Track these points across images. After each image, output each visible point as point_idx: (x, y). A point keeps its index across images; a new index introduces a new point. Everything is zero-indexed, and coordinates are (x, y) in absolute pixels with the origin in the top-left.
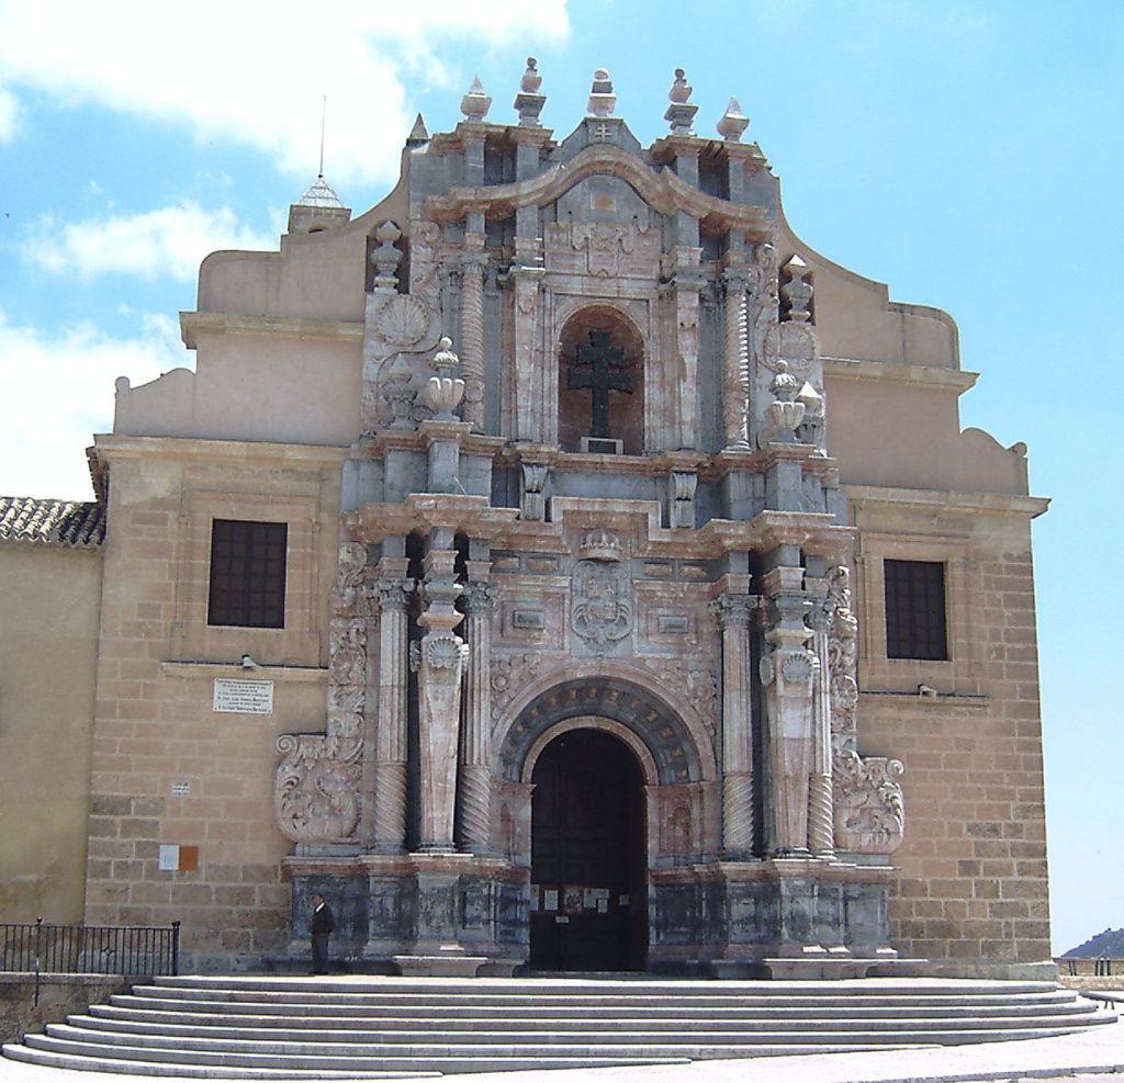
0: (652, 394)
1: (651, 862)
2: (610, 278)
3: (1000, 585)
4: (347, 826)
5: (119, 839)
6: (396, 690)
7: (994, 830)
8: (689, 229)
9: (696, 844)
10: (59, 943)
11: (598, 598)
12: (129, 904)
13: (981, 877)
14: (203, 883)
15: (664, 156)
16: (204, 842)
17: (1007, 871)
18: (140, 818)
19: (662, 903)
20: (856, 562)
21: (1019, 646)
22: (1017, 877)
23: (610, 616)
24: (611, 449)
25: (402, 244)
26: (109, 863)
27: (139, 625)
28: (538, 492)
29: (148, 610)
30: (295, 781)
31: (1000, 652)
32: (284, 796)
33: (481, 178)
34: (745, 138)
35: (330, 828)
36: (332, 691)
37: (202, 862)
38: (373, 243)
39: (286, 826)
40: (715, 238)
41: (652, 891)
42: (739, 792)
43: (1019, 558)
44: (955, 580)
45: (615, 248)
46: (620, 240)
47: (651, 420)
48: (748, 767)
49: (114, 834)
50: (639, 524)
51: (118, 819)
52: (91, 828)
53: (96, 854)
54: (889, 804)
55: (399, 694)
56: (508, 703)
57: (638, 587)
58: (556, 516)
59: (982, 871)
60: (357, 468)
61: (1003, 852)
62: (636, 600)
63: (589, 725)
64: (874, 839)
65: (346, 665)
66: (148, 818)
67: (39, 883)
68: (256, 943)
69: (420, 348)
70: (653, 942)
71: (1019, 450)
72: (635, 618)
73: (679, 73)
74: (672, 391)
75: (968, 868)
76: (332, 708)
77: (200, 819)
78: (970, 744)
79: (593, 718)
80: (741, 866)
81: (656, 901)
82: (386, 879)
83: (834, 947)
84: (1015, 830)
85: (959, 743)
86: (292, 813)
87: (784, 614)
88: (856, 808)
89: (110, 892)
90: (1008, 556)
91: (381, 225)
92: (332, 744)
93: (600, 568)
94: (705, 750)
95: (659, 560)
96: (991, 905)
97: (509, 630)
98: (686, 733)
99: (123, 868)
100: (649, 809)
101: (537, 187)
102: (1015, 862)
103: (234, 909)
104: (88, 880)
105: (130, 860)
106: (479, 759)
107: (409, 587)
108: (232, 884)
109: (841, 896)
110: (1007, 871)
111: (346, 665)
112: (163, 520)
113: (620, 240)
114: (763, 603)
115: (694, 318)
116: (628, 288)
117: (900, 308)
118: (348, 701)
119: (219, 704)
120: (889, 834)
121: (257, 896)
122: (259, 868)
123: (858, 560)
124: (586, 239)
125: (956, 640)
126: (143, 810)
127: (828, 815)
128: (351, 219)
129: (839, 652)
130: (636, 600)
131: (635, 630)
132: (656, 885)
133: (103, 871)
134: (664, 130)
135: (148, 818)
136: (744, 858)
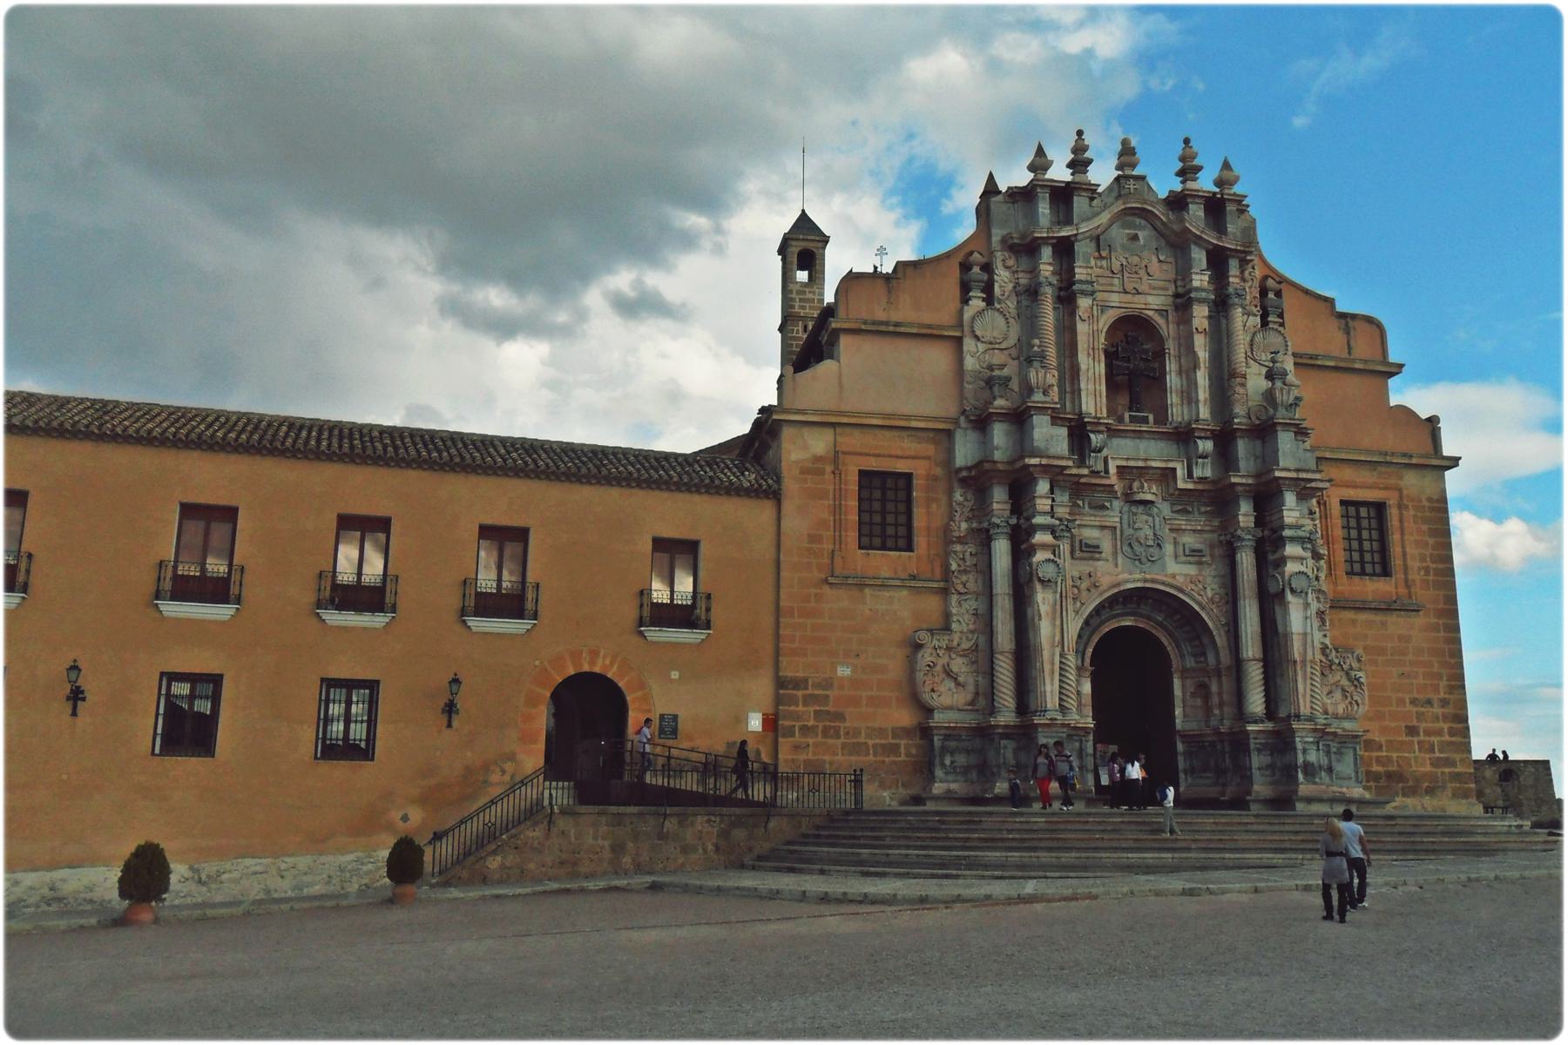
4: (970, 697)
7: (1429, 702)
8: (1199, 257)
12: (810, 756)
13: (1422, 737)
15: (1177, 202)
17: (1439, 733)
19: (1188, 754)
22: (1447, 738)
24: (1145, 420)
25: (988, 268)
29: (814, 538)
33: (1032, 229)
34: (1238, 189)
38: (965, 267)
40: (1218, 261)
41: (1180, 747)
43: (1438, 501)
48: (1259, 655)
51: (800, 693)
58: (1112, 470)
61: (1437, 719)
73: (1187, 141)
74: (1188, 378)
75: (1412, 731)
76: (954, 611)
78: (1407, 639)
84: (1444, 703)
85: (1401, 638)
89: (796, 748)
90: (1430, 500)
91: (971, 253)
93: (1141, 509)
94: (1221, 640)
97: (1078, 554)
99: (806, 730)
102: (1446, 726)
105: (810, 723)
107: (1014, 521)
110: (1439, 733)
112: (820, 472)
115: (1205, 324)
116: (1153, 302)
117: (1343, 316)
118: (966, 605)
121: (902, 750)
122: (904, 729)
126: (818, 685)
133: (790, 732)
134: (1176, 185)
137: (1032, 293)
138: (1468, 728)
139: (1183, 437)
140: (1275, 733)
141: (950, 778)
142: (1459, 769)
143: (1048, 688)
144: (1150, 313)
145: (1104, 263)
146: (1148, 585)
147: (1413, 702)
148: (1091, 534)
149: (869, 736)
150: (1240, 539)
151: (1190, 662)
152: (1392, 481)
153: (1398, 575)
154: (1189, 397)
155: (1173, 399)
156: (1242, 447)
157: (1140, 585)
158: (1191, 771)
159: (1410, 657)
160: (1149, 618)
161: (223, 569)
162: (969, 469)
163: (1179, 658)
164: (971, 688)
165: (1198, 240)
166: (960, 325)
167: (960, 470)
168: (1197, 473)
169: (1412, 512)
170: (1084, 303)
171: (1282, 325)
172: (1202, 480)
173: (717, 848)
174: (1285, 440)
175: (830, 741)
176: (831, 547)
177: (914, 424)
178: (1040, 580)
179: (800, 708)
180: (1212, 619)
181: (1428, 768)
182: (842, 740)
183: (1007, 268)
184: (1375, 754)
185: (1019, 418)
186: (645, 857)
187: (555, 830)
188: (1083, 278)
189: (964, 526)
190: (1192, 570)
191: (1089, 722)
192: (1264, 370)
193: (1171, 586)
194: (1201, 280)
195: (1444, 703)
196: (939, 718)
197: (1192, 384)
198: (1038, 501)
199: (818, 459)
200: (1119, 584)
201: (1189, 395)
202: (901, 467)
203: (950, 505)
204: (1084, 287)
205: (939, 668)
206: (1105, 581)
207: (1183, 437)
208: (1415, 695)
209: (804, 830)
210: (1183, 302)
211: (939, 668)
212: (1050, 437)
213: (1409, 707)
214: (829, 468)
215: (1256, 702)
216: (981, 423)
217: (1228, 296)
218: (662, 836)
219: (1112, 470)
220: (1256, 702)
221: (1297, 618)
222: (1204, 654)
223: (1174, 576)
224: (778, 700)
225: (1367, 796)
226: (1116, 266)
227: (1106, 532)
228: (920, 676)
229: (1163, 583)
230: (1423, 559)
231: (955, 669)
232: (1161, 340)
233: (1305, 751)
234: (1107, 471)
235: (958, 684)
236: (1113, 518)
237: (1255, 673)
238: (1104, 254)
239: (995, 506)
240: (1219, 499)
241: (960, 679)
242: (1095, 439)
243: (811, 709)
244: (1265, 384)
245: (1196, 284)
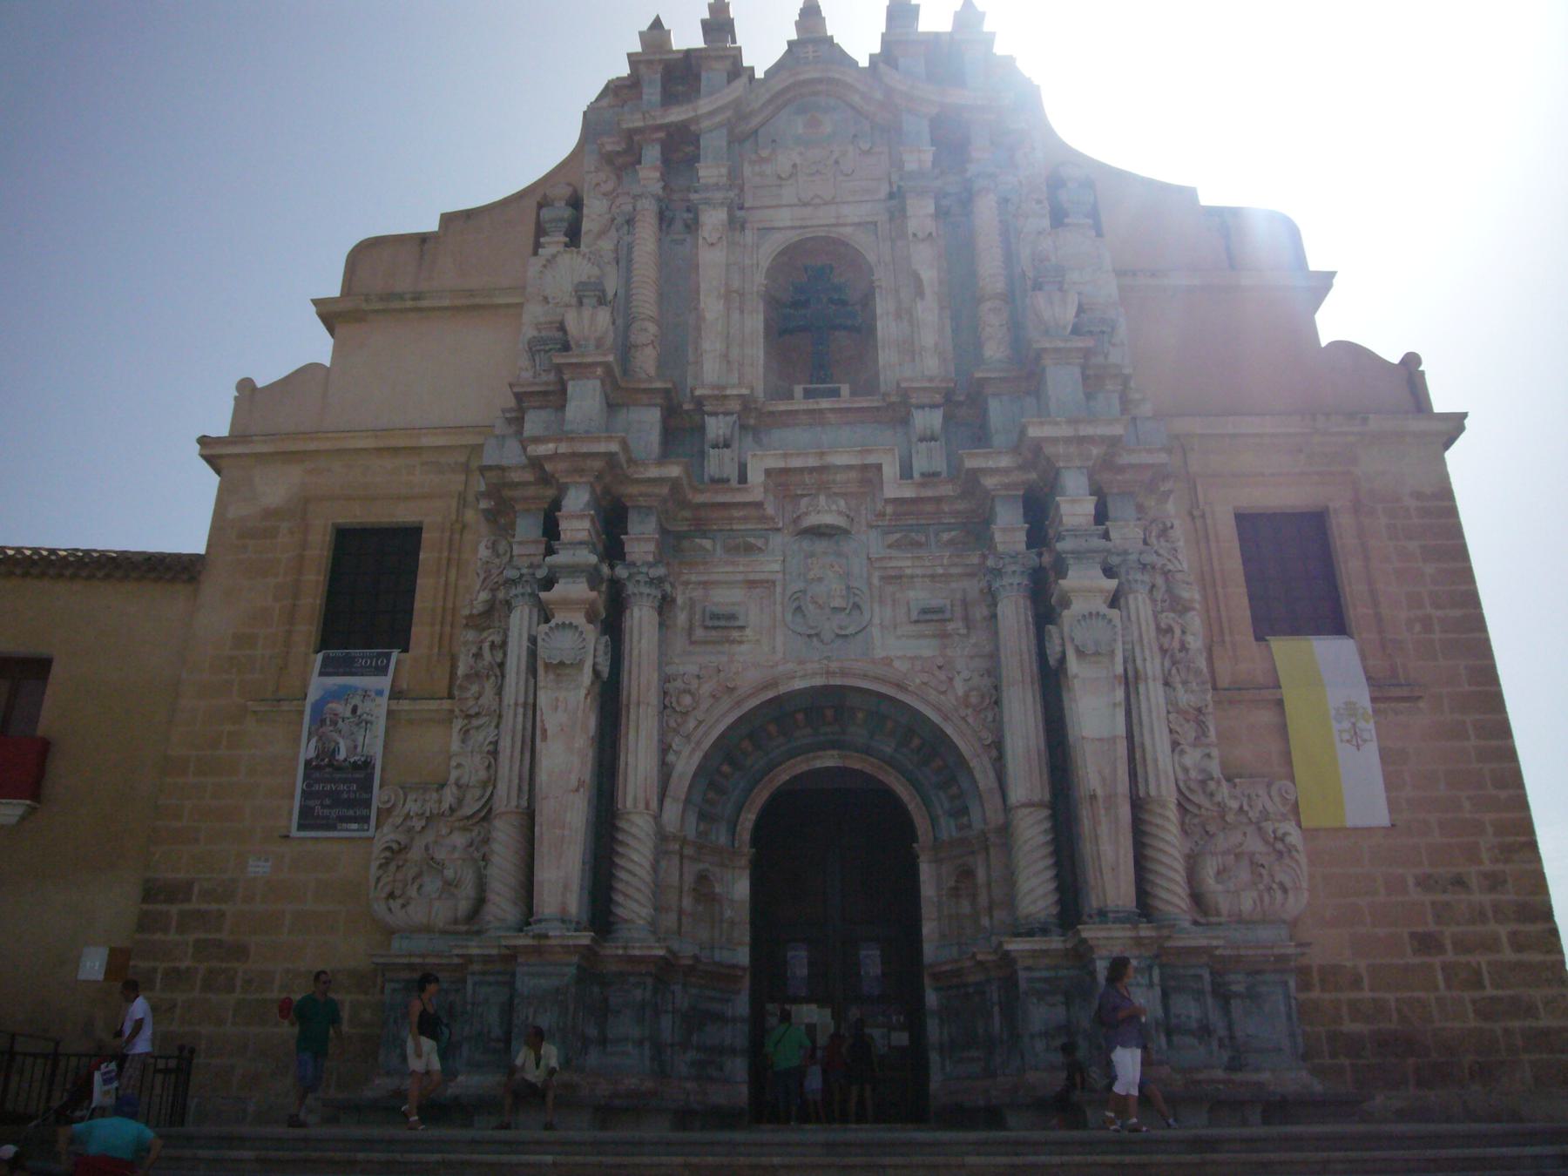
0: (887, 328)
2: (826, 203)
4: (464, 906)
5: (173, 936)
6: (521, 710)
9: (985, 921)
11: (820, 580)
13: (1450, 956)
17: (1491, 945)
18: (204, 906)
20: (1193, 518)
22: (1509, 955)
23: (838, 603)
25: (576, 203)
26: (155, 970)
28: (727, 445)
30: (395, 846)
32: (381, 866)
35: (442, 913)
36: (458, 724)
39: (380, 908)
41: (932, 998)
42: (1032, 832)
46: (837, 162)
47: (886, 357)
48: (1042, 793)
50: (870, 475)
51: (174, 909)
54: (1279, 846)
55: (525, 715)
56: (696, 728)
57: (877, 565)
58: (756, 476)
59: (1449, 947)
62: (876, 581)
63: (830, 763)
64: (1262, 900)
65: (475, 688)
66: (214, 906)
71: (1411, 361)
72: (876, 608)
79: (835, 752)
80: (1036, 943)
82: (491, 979)
84: (1494, 882)
86: (387, 889)
87: (1071, 561)
88: (1227, 852)
90: (1418, 495)
92: (449, 796)
93: (821, 545)
96: (1474, 1002)
97: (699, 633)
98: (962, 762)
100: (922, 878)
101: (720, 103)
102: (1503, 931)
105: (183, 965)
106: (635, 799)
109: (1208, 988)
111: (475, 688)
113: (837, 162)
114: (1047, 559)
120: (1285, 890)
123: (1196, 513)
124: (794, 166)
127: (1176, 870)
129: (1178, 632)
130: (876, 581)
131: (876, 621)
132: (936, 989)
135: (214, 906)
136: (1044, 931)
138: (1554, 932)
142: (1545, 1022)
146: (837, 681)
147: (1425, 883)
160: (868, 751)
161: (901, 1038)
172: (930, 477)
181: (1473, 1022)
190: (927, 649)
191: (743, 956)
193: (884, 681)
195: (1494, 882)
199: (269, 513)
200: (774, 683)
202: (404, 515)
223: (888, 662)
224: (145, 923)
225: (1318, 1087)
229: (865, 676)
234: (743, 479)
236: (769, 566)
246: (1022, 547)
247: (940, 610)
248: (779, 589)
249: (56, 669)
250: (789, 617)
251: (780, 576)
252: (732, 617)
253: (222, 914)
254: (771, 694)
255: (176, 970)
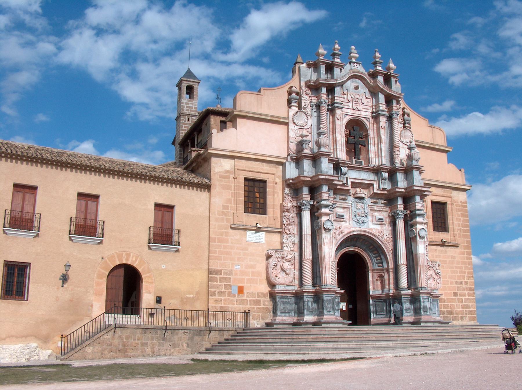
1: (371, 293)
3: (460, 210)
5: (219, 283)
7: (461, 283)
10: (200, 318)
12: (223, 305)
13: (459, 297)
14: (245, 298)
16: (245, 285)
18: (225, 276)
21: (465, 229)
22: (467, 297)
23: (363, 215)
26: (216, 291)
27: (223, 212)
29: (225, 207)
31: (460, 229)
37: (245, 291)
41: (371, 302)
43: (463, 203)
44: (449, 206)
45: (360, 101)
48: (405, 263)
49: (217, 282)
51: (218, 276)
52: (209, 279)
53: (212, 288)
60: (290, 164)
61: (464, 290)
66: (228, 276)
67: (193, 297)
68: (262, 318)
69: (305, 127)
70: (372, 317)
76: (285, 241)
77: (243, 277)
81: (373, 305)
83: (503, 240)
89: (216, 301)
90: (461, 202)
94: (390, 257)
95: (375, 196)
99: (220, 293)
102: (467, 292)
103: (255, 307)
104: (210, 297)
105: (222, 290)
108: (254, 299)
110: (465, 295)
112: (228, 178)
116: (365, 113)
118: (289, 239)
119: (248, 239)
121: (262, 302)
122: (262, 293)
125: (450, 226)
126: (226, 273)
128: (380, 94)
133: (214, 294)
135: (228, 276)
137: (318, 106)
139: (377, 171)
140: (412, 295)
141: (283, 315)
142: (471, 309)
143: (328, 275)
144: (363, 119)
145: (345, 96)
147: (456, 283)
148: (340, 211)
149: (248, 296)
150: (398, 214)
151: (376, 267)
152: (449, 194)
153: (451, 232)
154: (379, 155)
155: (372, 155)
156: (400, 177)
157: (359, 233)
158: (376, 312)
159: (455, 265)
162: (293, 179)
163: (371, 264)
164: (292, 275)
165: (382, 91)
166: (288, 118)
167: (289, 179)
168: (382, 187)
169: (455, 207)
170: (338, 112)
171: (410, 128)
172: (384, 189)
173: (188, 345)
174: (416, 173)
175: (231, 298)
176: (232, 211)
177: (268, 159)
178: (325, 229)
179: (219, 283)
180: (388, 248)
182: (236, 298)
183: (307, 95)
184: (442, 304)
185: (315, 159)
186: (156, 349)
187: (117, 335)
188: (338, 101)
189: (290, 204)
192: (407, 147)
194: (383, 107)
196: (279, 288)
197: (379, 149)
198: (323, 194)
199: (227, 172)
200: (351, 232)
201: (377, 154)
202: (262, 177)
203: (283, 195)
204: (339, 105)
205: (279, 267)
206: (346, 231)
207: (377, 171)
208: (456, 280)
209: (225, 337)
210: (376, 116)
211: (279, 267)
212: (326, 166)
213: (454, 285)
214: (232, 176)
215: (404, 282)
216: (298, 161)
217: (393, 114)
218: (164, 339)
219: (349, 184)
220: (404, 282)
221: (421, 248)
222: (382, 263)
223: (371, 229)
226: (350, 99)
227: (345, 210)
228: (270, 270)
229: (368, 232)
230: (459, 226)
231: (285, 267)
232: (367, 130)
233: (424, 302)
234: (347, 183)
235: (286, 274)
237: (403, 270)
238: (345, 92)
239: (304, 196)
240: (390, 199)
241: (287, 271)
242: (344, 169)
243: (223, 284)
244: (408, 151)
245: (381, 108)
246: (403, 209)
247: (382, 219)
248: (351, 210)
249: (101, 198)
250: (353, 216)
251: (350, 207)
252: (343, 216)
253: (230, 278)
254: (349, 235)
255: (221, 291)
